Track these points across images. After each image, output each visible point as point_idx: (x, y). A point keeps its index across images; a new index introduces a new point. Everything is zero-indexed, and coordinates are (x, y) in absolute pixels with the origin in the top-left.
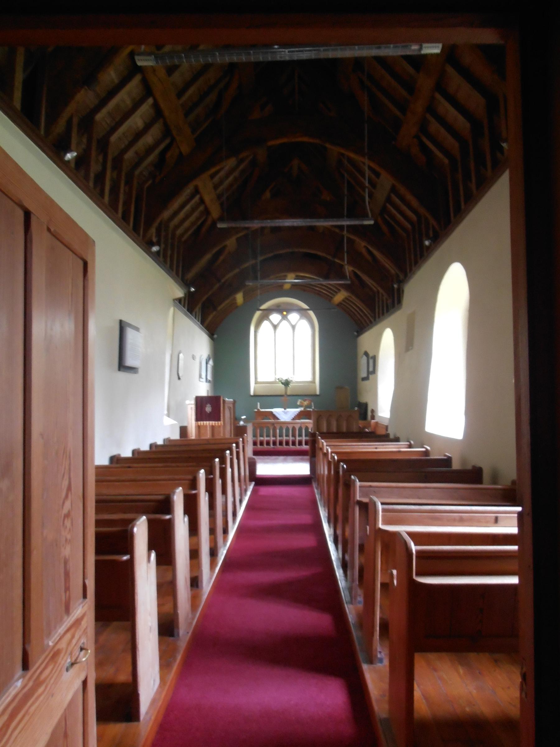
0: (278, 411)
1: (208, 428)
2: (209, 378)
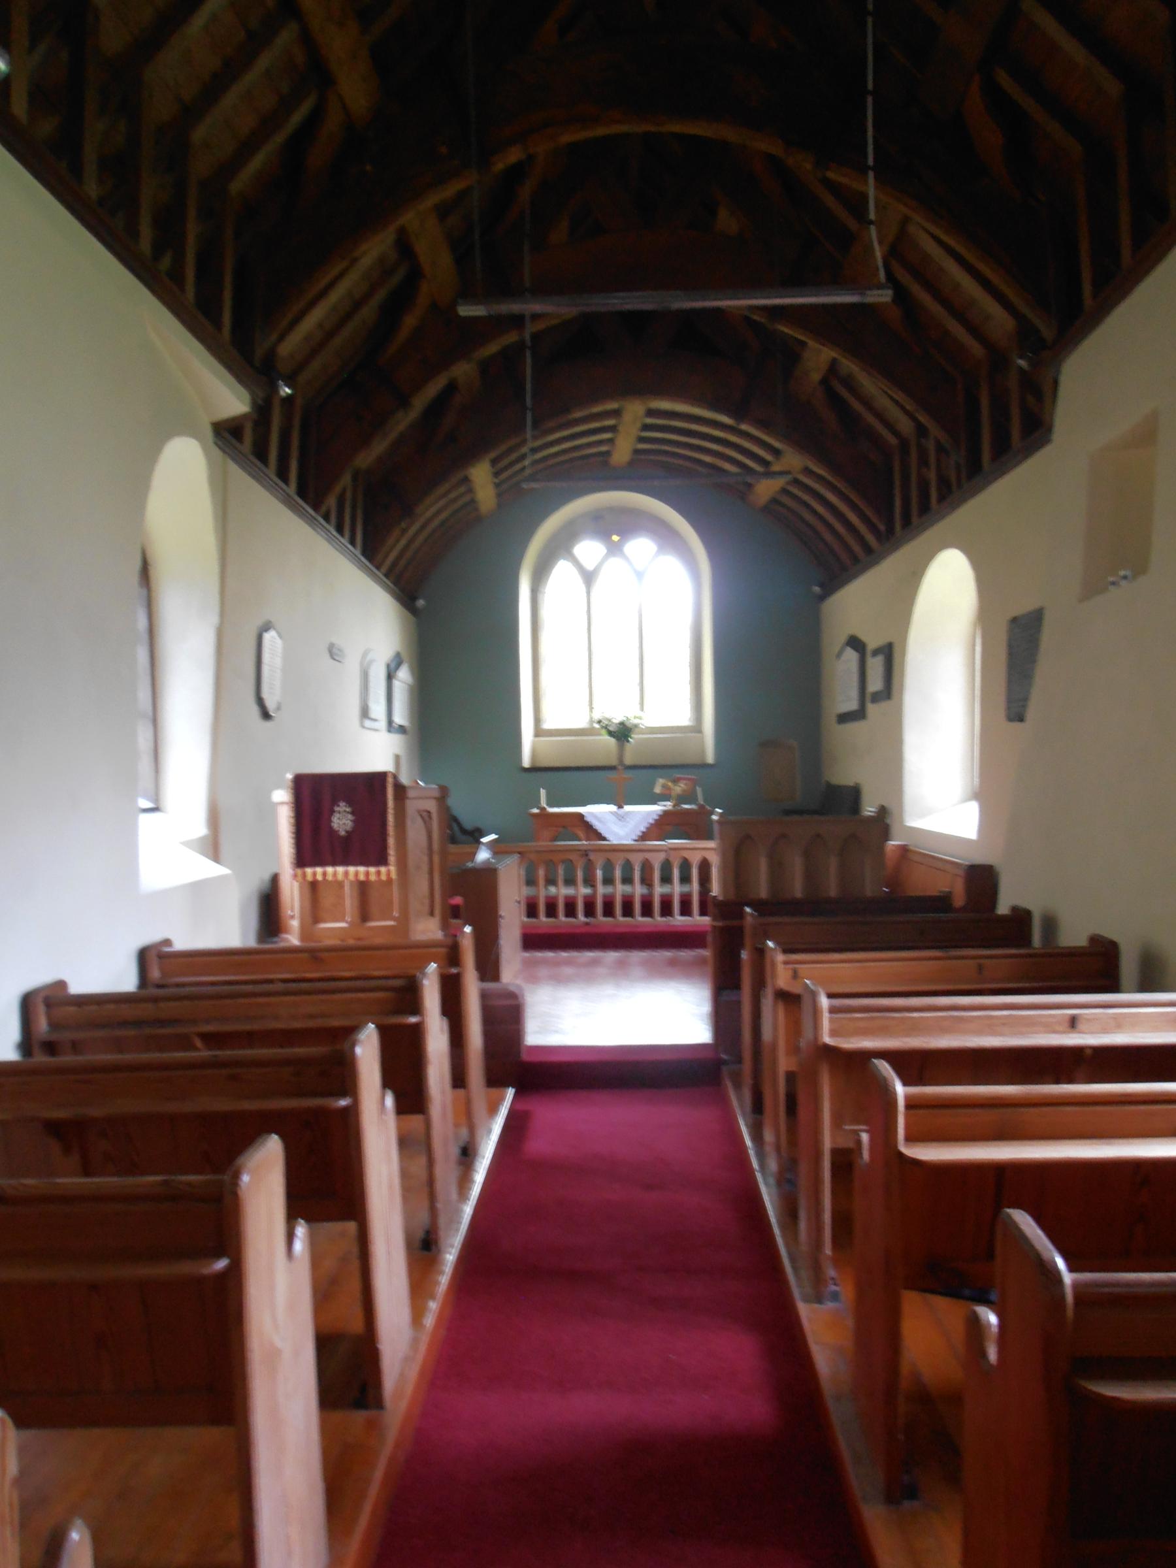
0: (598, 813)
1: (347, 888)
2: (400, 718)
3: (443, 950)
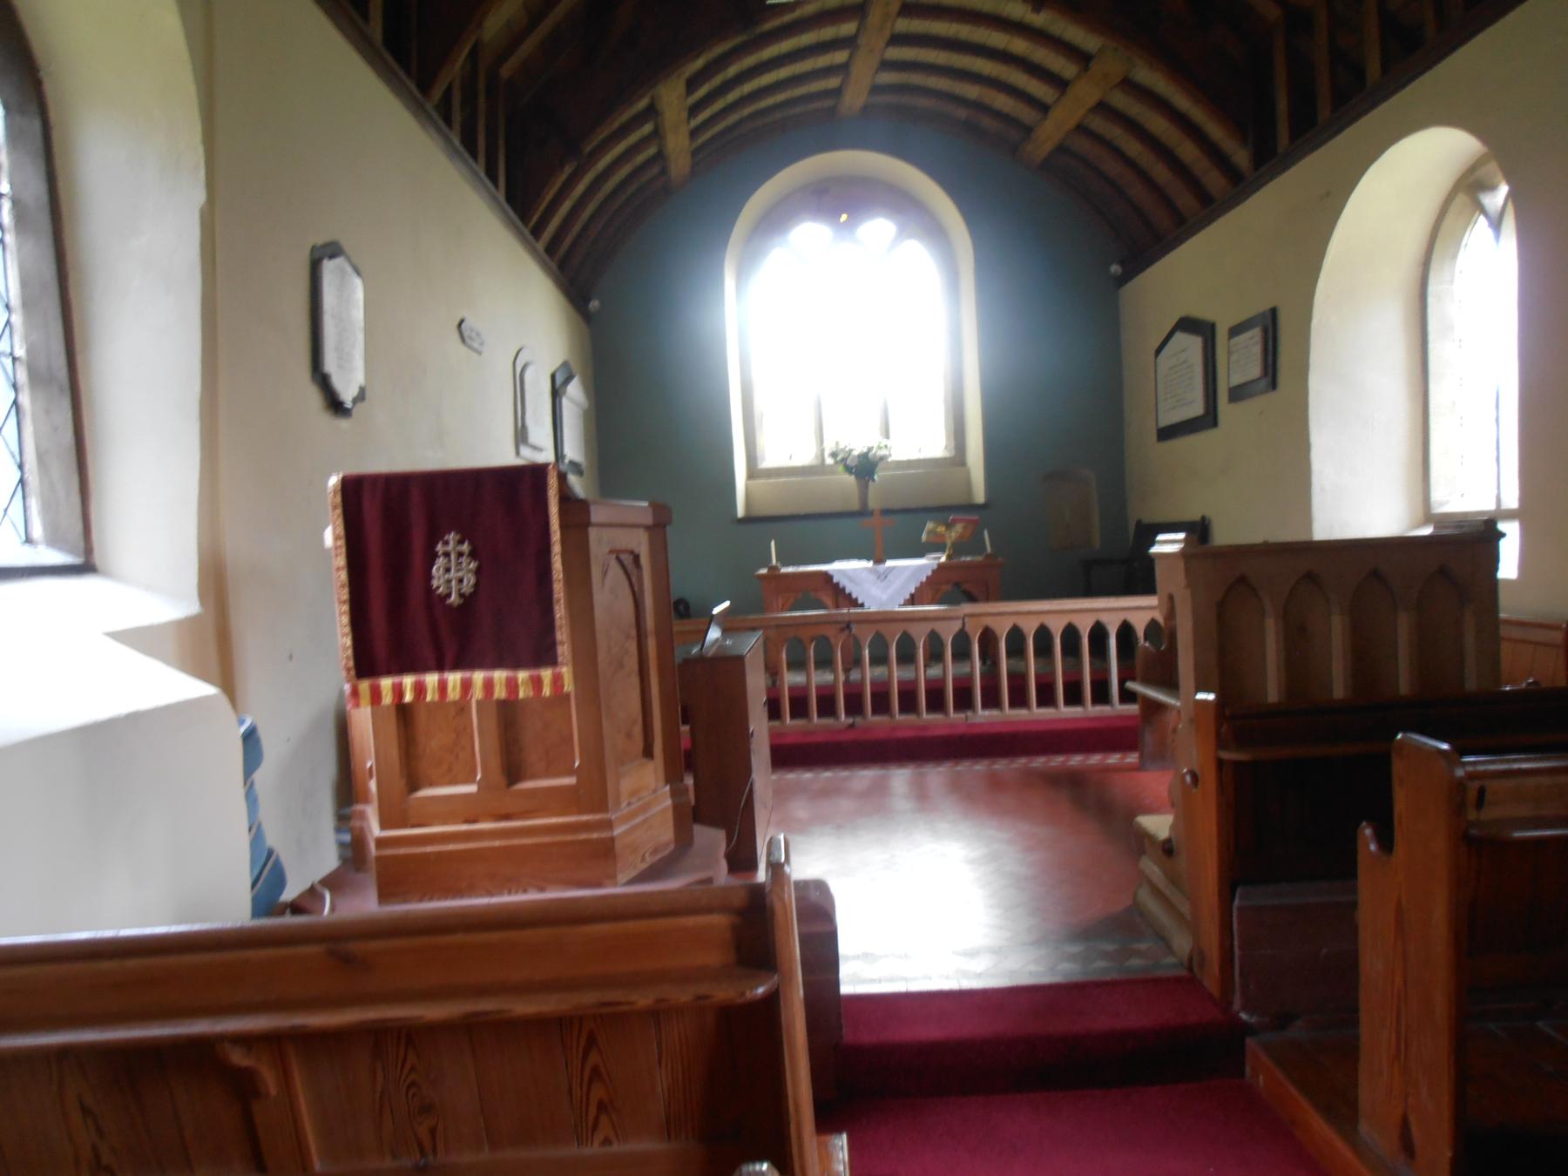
3: (719, 920)
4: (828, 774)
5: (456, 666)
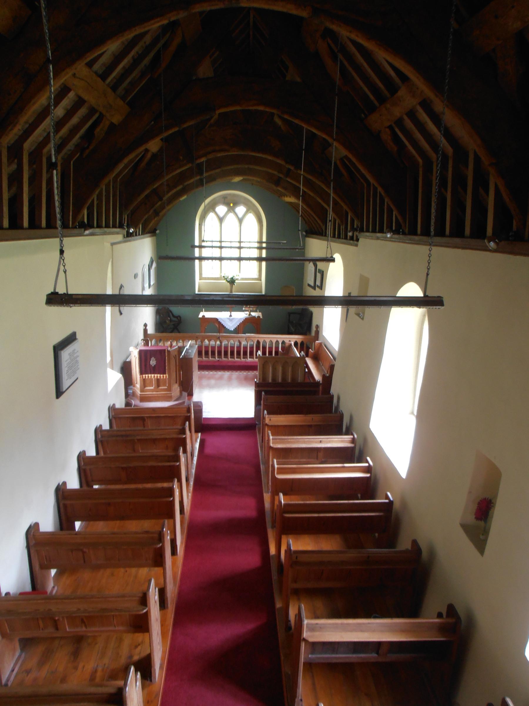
3: (186, 409)
4: (211, 373)
5: (153, 373)
